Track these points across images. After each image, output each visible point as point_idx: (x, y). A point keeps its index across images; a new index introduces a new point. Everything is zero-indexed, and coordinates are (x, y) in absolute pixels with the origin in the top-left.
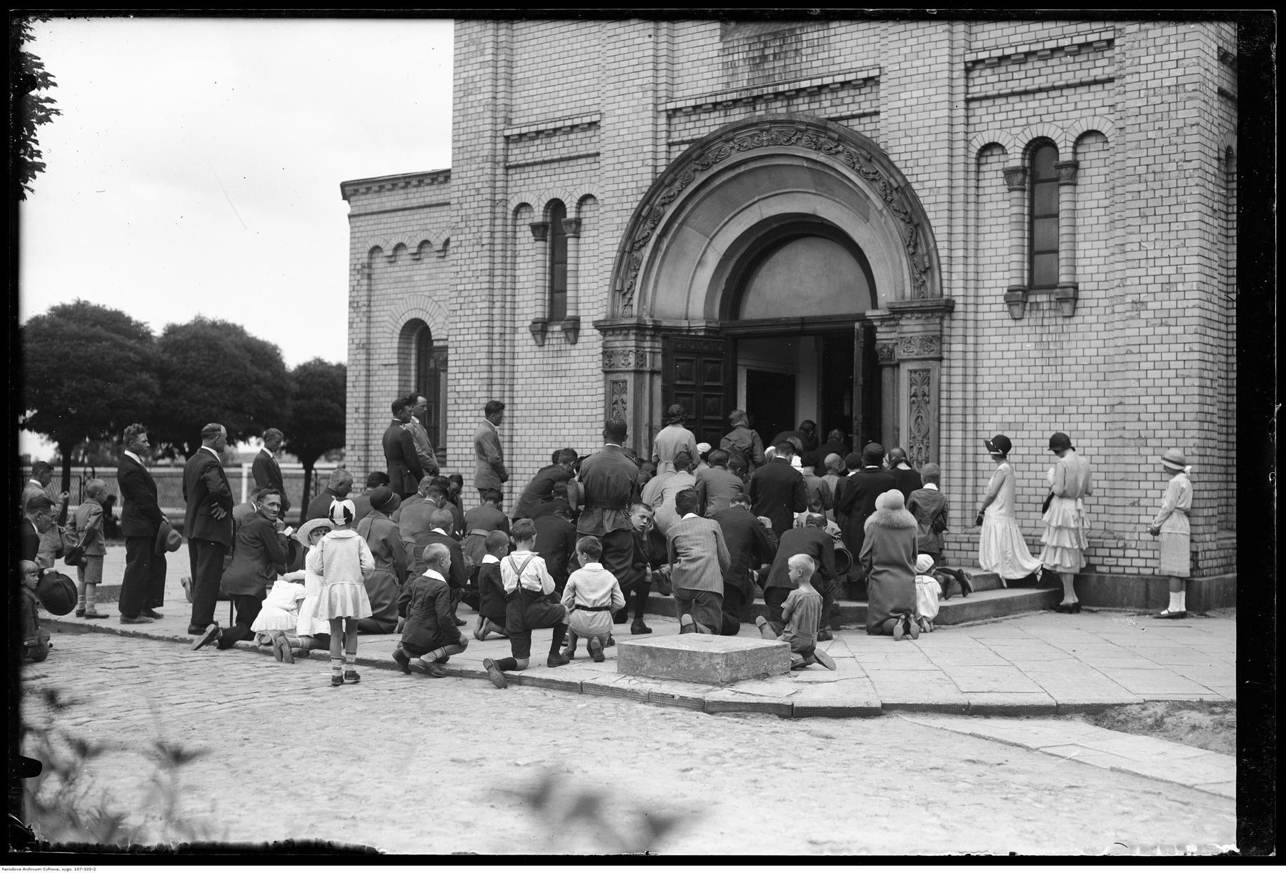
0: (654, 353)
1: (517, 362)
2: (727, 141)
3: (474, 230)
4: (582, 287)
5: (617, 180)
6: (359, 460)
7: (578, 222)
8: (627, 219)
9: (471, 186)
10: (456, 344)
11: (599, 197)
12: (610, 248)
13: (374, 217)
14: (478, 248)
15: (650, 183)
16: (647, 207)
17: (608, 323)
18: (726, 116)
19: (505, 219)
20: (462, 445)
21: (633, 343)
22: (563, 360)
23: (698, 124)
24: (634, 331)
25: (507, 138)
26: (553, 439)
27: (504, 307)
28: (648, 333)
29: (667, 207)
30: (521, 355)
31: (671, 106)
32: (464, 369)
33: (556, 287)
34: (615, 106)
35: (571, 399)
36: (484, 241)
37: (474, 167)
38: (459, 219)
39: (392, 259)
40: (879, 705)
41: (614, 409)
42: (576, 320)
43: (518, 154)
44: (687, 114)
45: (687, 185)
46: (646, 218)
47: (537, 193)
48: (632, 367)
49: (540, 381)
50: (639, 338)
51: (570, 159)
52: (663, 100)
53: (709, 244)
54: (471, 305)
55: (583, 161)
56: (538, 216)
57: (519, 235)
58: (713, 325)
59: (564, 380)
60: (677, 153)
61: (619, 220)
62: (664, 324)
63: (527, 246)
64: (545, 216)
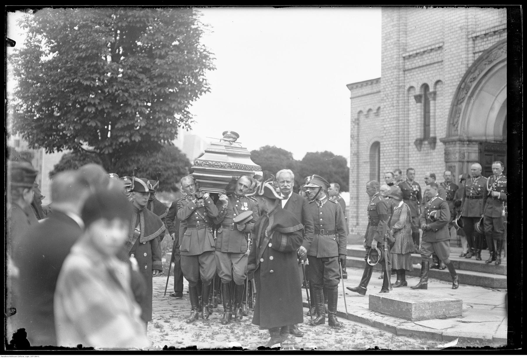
1: (410, 159)
2: (499, 49)
4: (437, 123)
6: (354, 204)
7: (435, 93)
8: (455, 90)
11: (443, 81)
13: (359, 98)
15: (465, 72)
16: (463, 84)
18: (500, 37)
19: (404, 94)
21: (458, 148)
23: (487, 42)
25: (404, 58)
27: (404, 134)
28: (465, 143)
31: (474, 35)
34: (449, 38)
37: (390, 72)
39: (367, 116)
40: (491, 338)
42: (435, 139)
43: (409, 65)
44: (482, 38)
45: (482, 71)
48: (457, 160)
51: (431, 64)
52: (471, 33)
53: (495, 99)
54: (389, 134)
55: (436, 65)
56: (418, 91)
60: (477, 56)
64: (420, 91)
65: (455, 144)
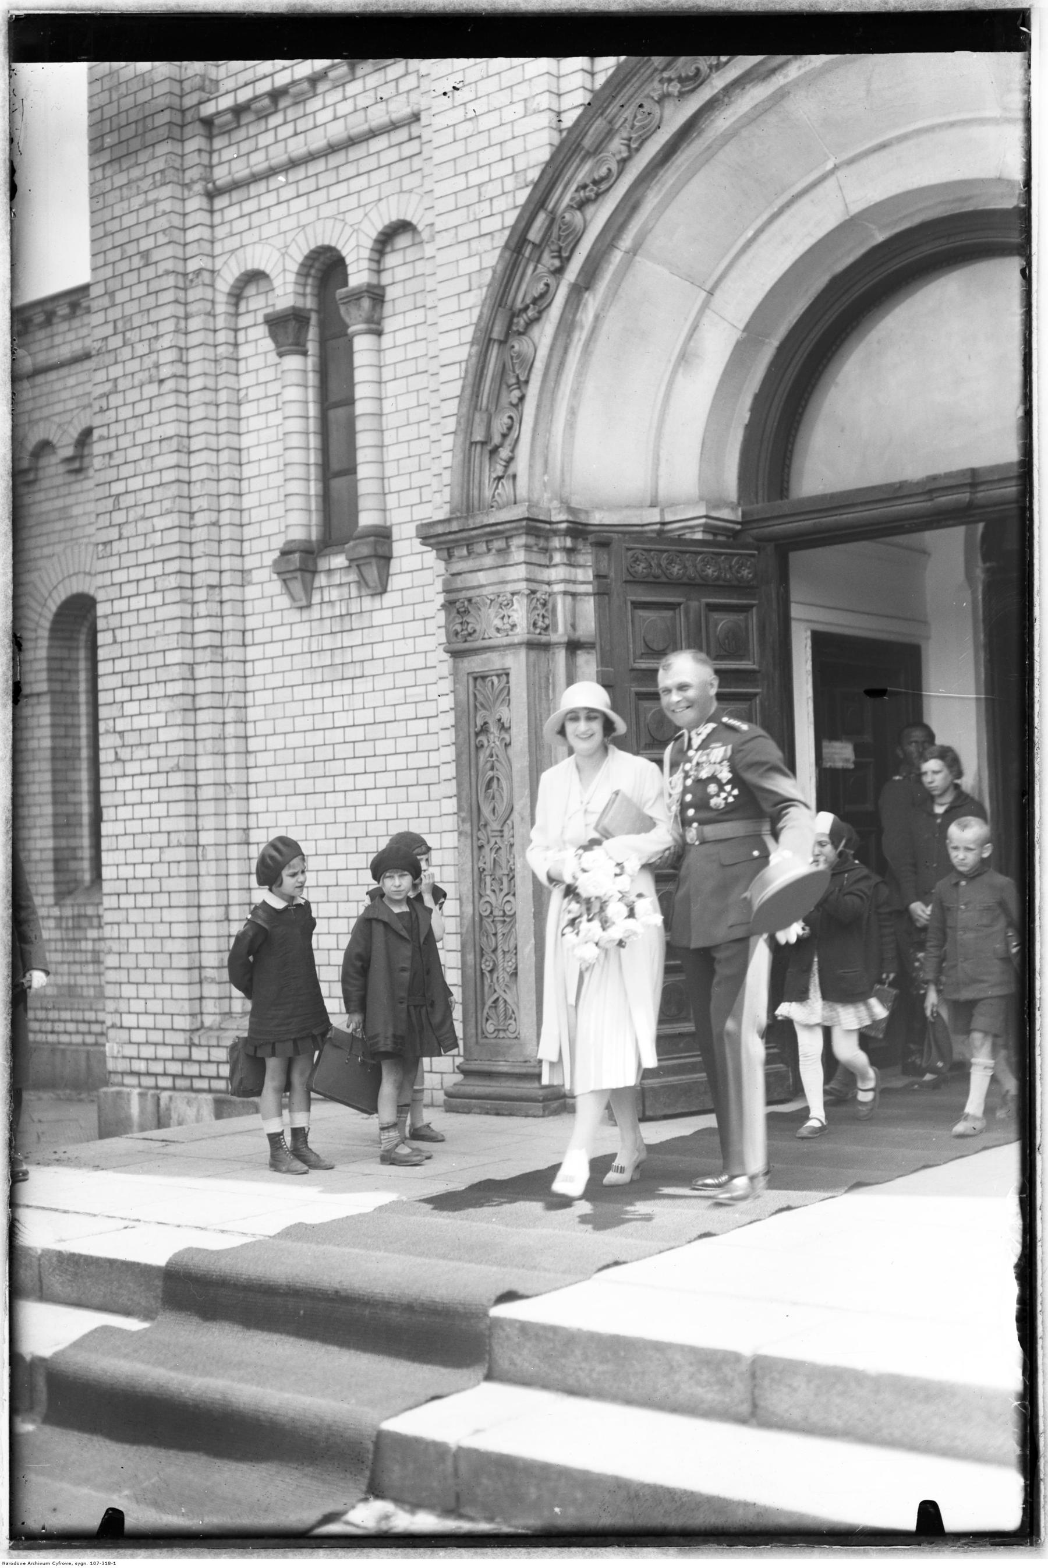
0: (574, 595)
3: (142, 349)
5: (464, 165)
7: (376, 295)
8: (492, 259)
9: (131, 249)
10: (114, 622)
12: (453, 338)
14: (151, 390)
16: (541, 218)
17: (455, 526)
20: (134, 856)
22: (355, 638)
24: (522, 540)
26: (338, 831)
28: (556, 542)
29: (590, 209)
30: (260, 636)
32: (131, 679)
33: (335, 466)
35: (378, 731)
36: (165, 372)
38: (109, 329)
41: (479, 747)
42: (383, 535)
46: (538, 247)
47: (279, 242)
48: (521, 633)
49: (304, 692)
50: (536, 558)
51: (352, 142)
53: (705, 305)
55: (379, 143)
57: (244, 351)
58: (725, 514)
59: (360, 685)
61: (473, 264)
62: (597, 518)
63: (273, 619)
65: (504, 552)
